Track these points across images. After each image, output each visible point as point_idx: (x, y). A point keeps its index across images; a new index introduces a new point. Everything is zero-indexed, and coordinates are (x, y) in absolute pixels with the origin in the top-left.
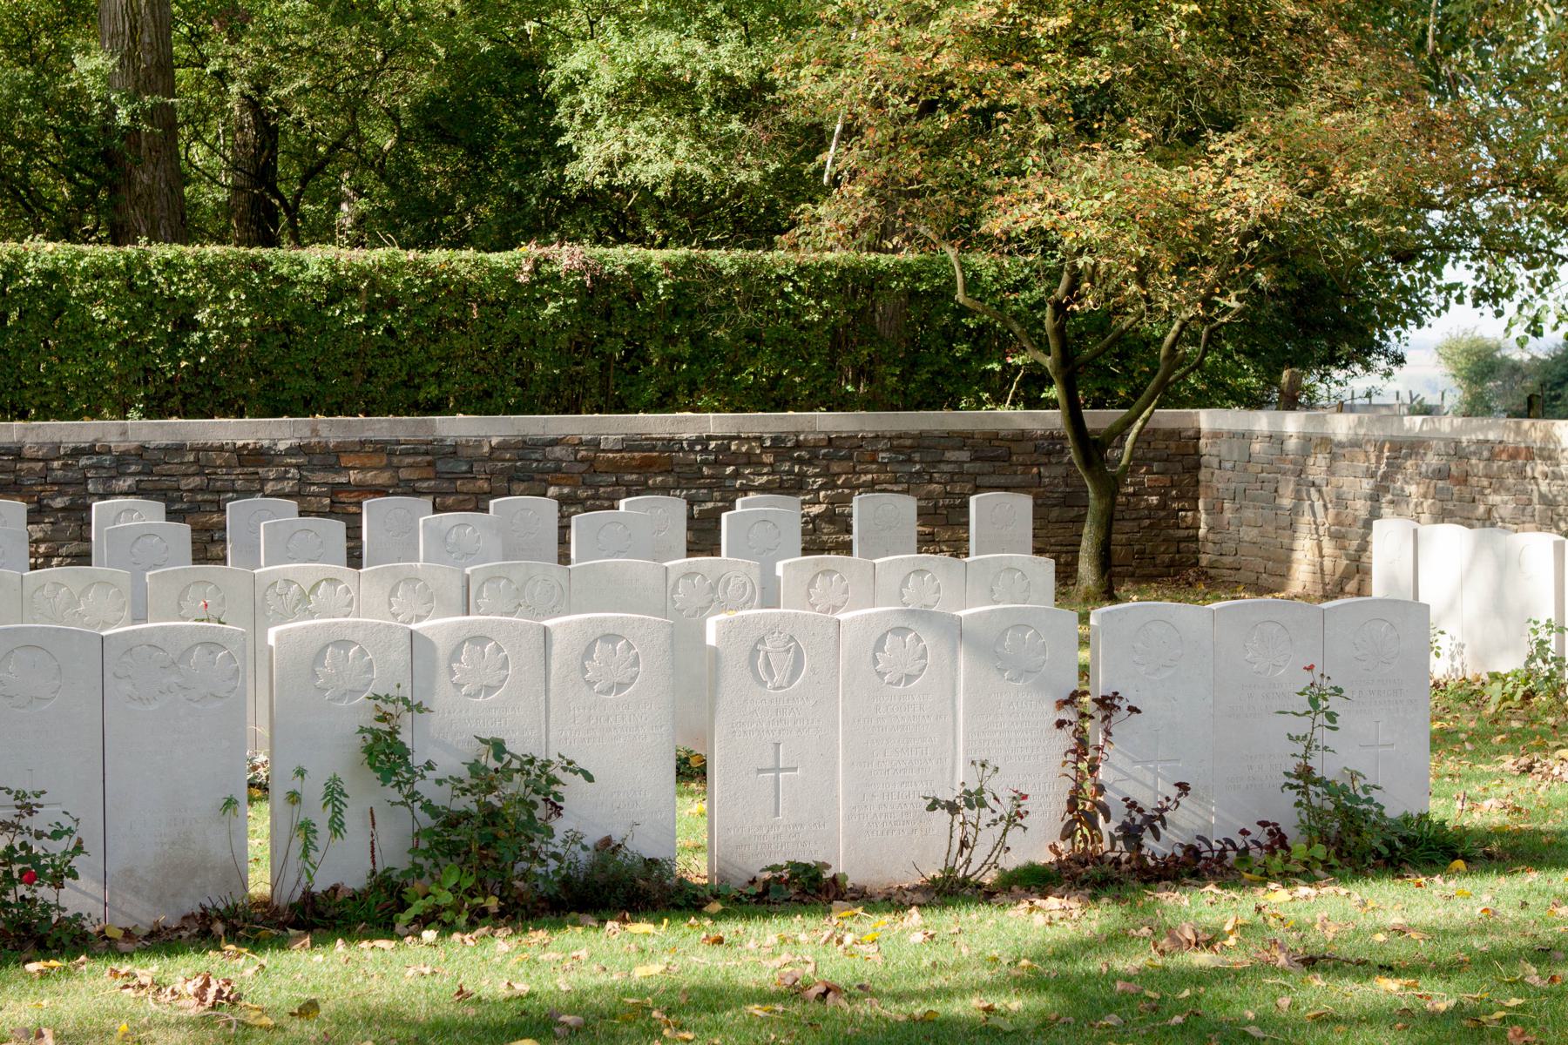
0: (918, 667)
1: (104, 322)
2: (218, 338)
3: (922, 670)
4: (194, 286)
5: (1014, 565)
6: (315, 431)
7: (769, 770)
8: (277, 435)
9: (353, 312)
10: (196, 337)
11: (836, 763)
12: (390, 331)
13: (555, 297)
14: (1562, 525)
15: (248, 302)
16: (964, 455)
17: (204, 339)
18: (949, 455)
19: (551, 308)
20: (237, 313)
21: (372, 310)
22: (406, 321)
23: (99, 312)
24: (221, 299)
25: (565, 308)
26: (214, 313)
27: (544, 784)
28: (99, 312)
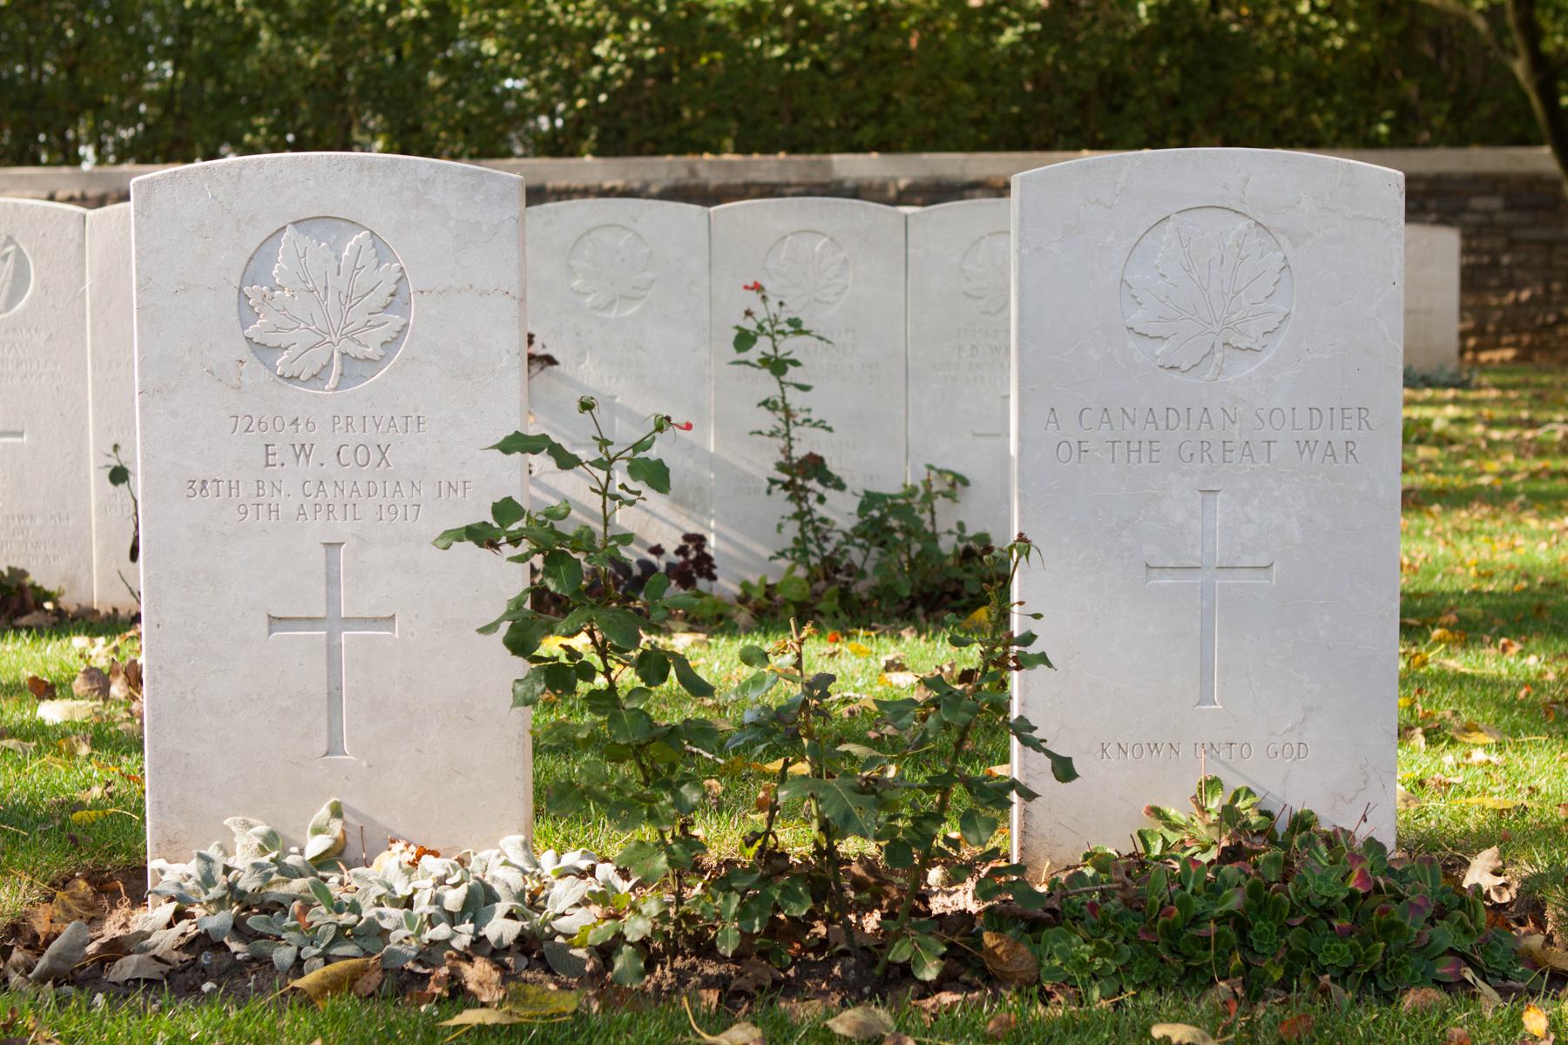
0: (381, 334)
1: (495, 57)
2: (619, 74)
3: (389, 345)
4: (592, 17)
6: (693, 172)
7: (332, 600)
8: (649, 176)
9: (774, 42)
10: (596, 71)
11: (84, 428)
12: (819, 65)
13: (1013, 23)
14: (5, 37)
15: (652, 32)
16: (1495, 203)
17: (604, 74)
19: (1009, 36)
20: (641, 45)
21: (795, 39)
22: (837, 52)
23: (489, 47)
24: (622, 29)
25: (1027, 36)
26: (614, 46)
27: (24, 574)
28: (489, 47)
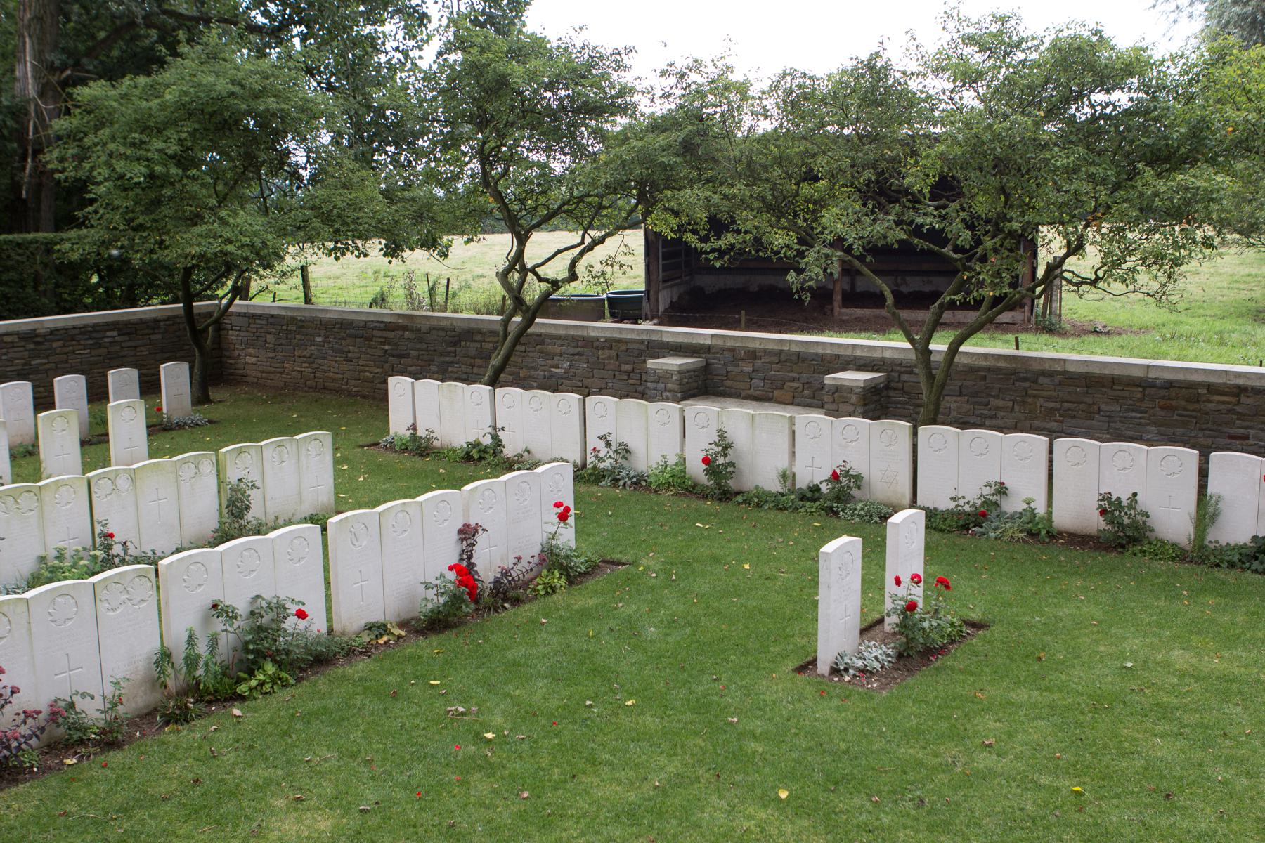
5: (199, 559)
16: (115, 333)
18: (109, 334)
